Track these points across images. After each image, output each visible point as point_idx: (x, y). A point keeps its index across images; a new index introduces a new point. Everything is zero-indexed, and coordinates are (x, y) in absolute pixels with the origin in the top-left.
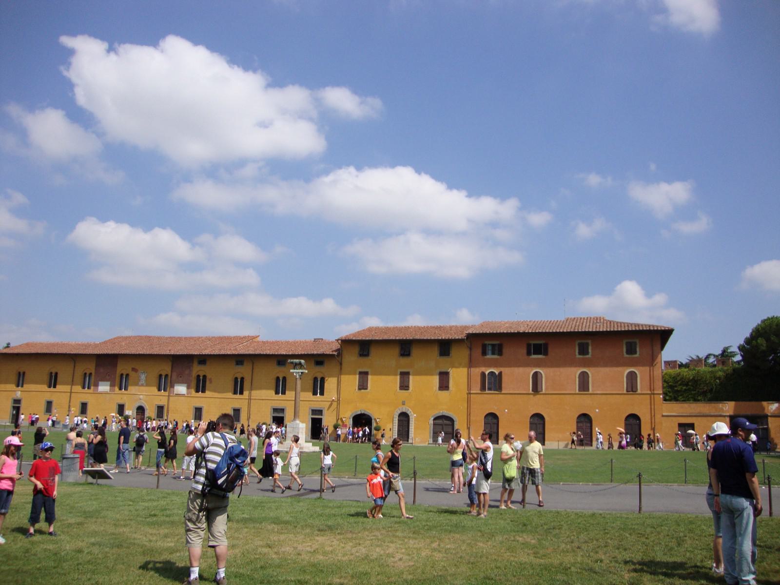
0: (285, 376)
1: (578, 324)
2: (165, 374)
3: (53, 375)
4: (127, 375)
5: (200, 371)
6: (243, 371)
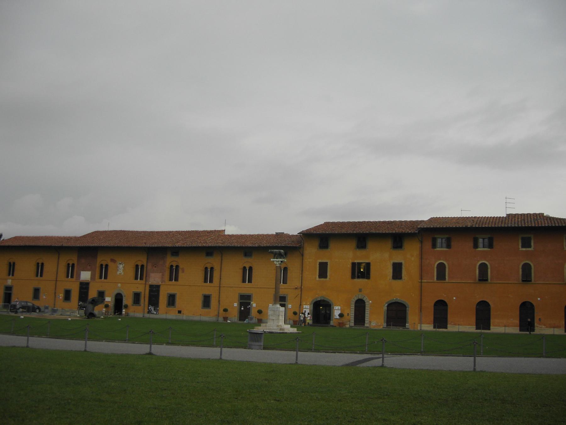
0: (251, 266)
1: (520, 220)
2: (210, 267)
3: (40, 265)
4: (107, 266)
5: (69, 260)
6: (214, 261)
